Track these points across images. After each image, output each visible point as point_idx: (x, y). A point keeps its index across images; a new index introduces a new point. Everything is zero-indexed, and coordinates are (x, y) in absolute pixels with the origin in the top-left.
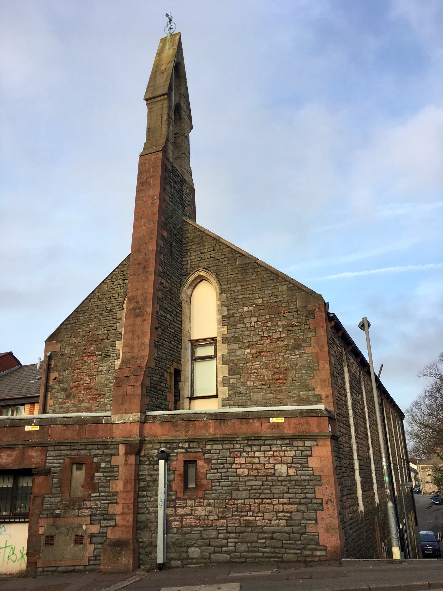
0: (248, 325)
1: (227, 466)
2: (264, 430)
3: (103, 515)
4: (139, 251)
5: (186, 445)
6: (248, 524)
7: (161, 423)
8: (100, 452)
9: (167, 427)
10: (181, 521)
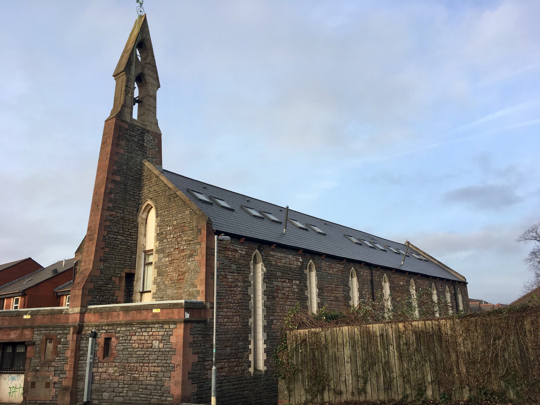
0: (169, 240)
1: (128, 341)
2: (150, 319)
3: (61, 370)
4: (96, 193)
5: (107, 328)
6: (135, 379)
7: (94, 313)
8: (61, 332)
9: (97, 315)
10: (100, 376)
